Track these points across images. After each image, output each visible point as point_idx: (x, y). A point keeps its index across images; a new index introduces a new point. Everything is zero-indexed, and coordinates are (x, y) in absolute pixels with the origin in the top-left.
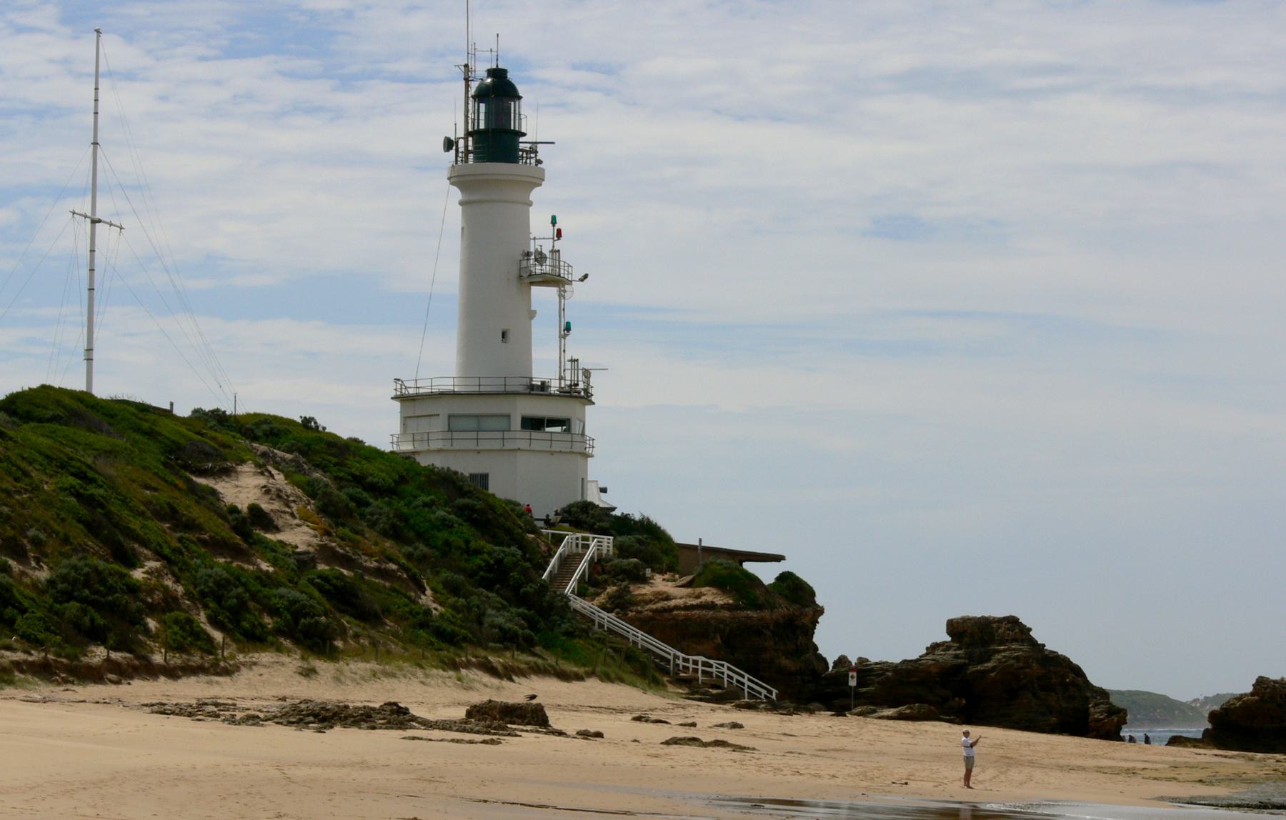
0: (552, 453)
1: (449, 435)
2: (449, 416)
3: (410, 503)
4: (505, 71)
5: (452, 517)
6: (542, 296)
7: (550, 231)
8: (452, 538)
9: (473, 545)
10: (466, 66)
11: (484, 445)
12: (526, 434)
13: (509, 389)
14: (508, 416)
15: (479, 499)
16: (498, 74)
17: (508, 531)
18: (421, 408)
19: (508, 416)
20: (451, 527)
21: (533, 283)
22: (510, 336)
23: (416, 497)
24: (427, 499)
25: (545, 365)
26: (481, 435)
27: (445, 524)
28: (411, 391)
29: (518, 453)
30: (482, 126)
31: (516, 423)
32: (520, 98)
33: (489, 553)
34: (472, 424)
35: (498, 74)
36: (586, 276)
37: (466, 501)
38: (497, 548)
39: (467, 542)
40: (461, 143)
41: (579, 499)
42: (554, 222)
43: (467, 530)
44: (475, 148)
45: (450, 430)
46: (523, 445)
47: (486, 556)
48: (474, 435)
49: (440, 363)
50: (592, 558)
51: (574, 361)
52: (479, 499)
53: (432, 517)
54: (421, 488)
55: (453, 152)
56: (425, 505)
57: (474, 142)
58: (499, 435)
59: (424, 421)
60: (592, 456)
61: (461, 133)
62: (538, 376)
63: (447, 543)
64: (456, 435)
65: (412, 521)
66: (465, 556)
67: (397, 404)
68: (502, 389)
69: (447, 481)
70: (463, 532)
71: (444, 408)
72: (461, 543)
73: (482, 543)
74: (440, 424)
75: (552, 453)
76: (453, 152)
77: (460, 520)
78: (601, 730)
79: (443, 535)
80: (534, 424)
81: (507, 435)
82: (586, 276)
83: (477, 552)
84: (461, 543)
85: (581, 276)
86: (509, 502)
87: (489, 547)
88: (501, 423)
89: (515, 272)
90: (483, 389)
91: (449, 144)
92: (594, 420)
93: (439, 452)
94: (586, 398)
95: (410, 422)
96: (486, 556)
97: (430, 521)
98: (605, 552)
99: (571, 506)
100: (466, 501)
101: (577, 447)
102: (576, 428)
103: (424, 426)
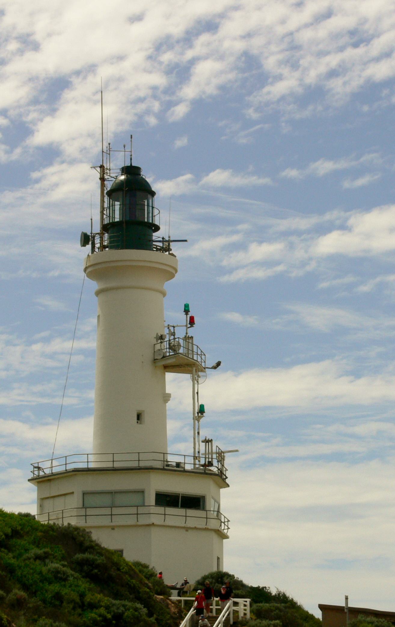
0: (187, 529)
1: (83, 512)
2: (84, 494)
3: (20, 555)
4: (138, 169)
5: (69, 571)
6: (176, 384)
7: (183, 319)
8: (65, 591)
9: (88, 598)
10: (102, 167)
11: (118, 521)
12: (161, 510)
13: (142, 464)
14: (143, 492)
15: (101, 554)
16: (131, 171)
17: (133, 590)
18: (56, 489)
19: (143, 492)
20: (65, 580)
21: (168, 368)
22: (146, 418)
23: (27, 550)
24: (40, 552)
25: (180, 448)
26: (115, 511)
27: (59, 577)
28: (48, 472)
29: (153, 530)
30: (117, 220)
31: (151, 499)
32: (153, 194)
33: (107, 608)
34: (107, 500)
35: (131, 171)
36: (219, 364)
37: (87, 555)
38: (117, 602)
39: (82, 596)
40: (97, 241)
41: (215, 569)
42: (187, 311)
43: (84, 585)
44: (110, 242)
45: (84, 507)
46: (157, 520)
47: (102, 611)
48: (108, 511)
49: (76, 439)
50: (227, 620)
51: (207, 441)
52: (101, 554)
53: (44, 569)
54: (37, 543)
55: (89, 247)
56: (37, 557)
57: (110, 238)
58: (133, 510)
59: (61, 500)
60: (227, 537)
61: (97, 229)
62: (173, 459)
63: (58, 596)
64: (90, 512)
65: (19, 573)
66: (79, 611)
67: (33, 487)
68: (135, 464)
69: (71, 540)
70: (79, 585)
71: (78, 486)
72: (75, 596)
73: (99, 596)
74: (75, 501)
75: (187, 529)
76: (89, 247)
77: (77, 575)
78: (217, 362)
79: (55, 587)
80: (166, 500)
81: (141, 510)
82: (219, 364)
83: (92, 606)
84: (75, 596)
85: (214, 364)
86: (138, 564)
87: (107, 600)
88: (135, 499)
89: (149, 356)
90: (117, 465)
91: (86, 239)
92: (230, 501)
93: (67, 514)
94: (221, 479)
95: (47, 503)
96: (102, 611)
97: (41, 573)
98: (241, 614)
99: (205, 578)
100: (87, 555)
101: (213, 524)
102: (210, 504)
103: (59, 503)
